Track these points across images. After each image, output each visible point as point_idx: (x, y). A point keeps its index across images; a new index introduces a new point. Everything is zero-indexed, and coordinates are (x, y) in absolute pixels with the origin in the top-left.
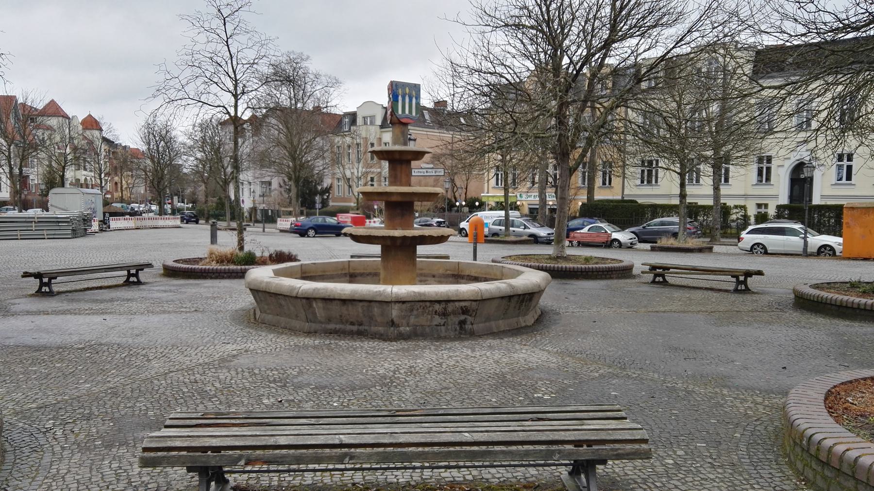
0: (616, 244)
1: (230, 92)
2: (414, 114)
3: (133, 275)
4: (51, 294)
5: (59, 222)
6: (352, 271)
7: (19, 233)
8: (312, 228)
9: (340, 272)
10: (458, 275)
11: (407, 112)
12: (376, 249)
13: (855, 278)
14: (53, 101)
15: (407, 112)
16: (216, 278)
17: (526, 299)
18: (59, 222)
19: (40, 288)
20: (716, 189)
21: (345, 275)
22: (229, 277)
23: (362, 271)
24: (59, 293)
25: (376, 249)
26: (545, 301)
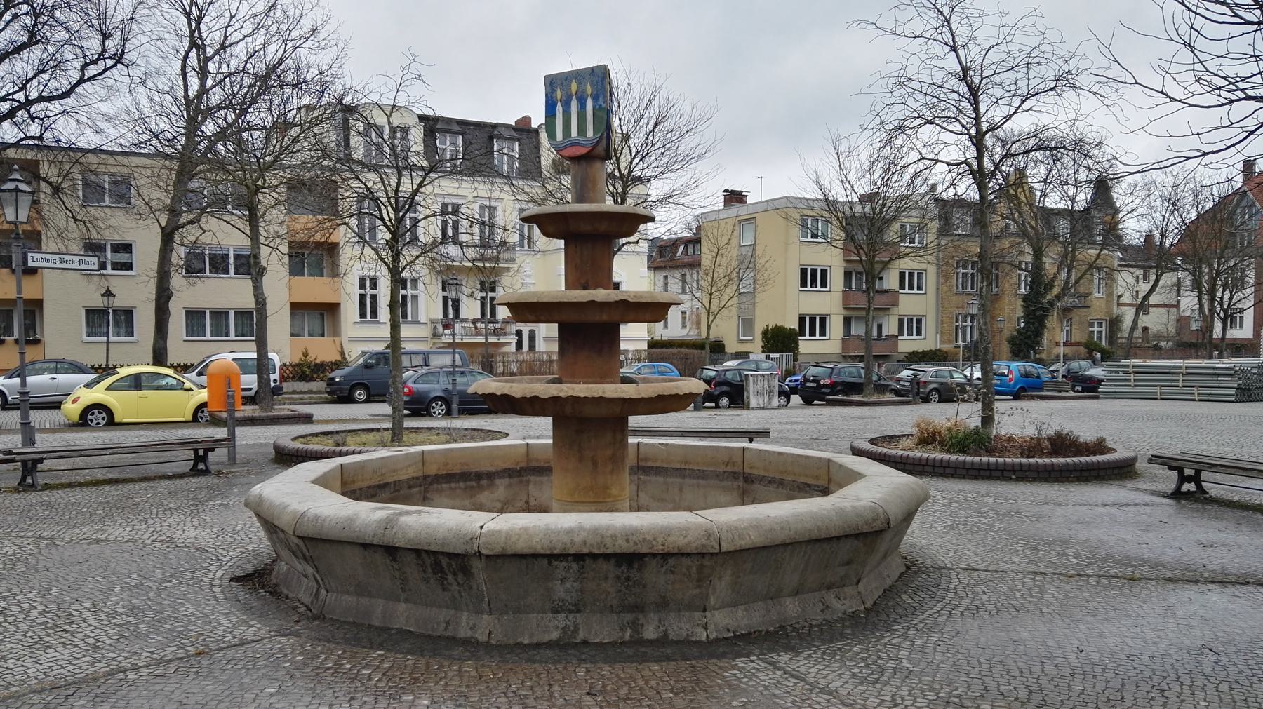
0: (97, 417)
1: (226, 38)
2: (590, 133)
3: (1189, 479)
4: (206, 472)
5: (1219, 375)
6: (747, 470)
7: (1158, 390)
8: (513, 374)
9: (722, 468)
10: (747, 481)
11: (574, 132)
12: (543, 425)
13: (640, 514)
14: (605, 69)
15: (574, 132)
16: (1034, 480)
17: (872, 537)
18: (1219, 375)
19: (195, 465)
20: (395, 327)
21: (735, 475)
22: (1046, 480)
23: (762, 473)
24: (1216, 501)
25: (543, 425)
26: (920, 537)
